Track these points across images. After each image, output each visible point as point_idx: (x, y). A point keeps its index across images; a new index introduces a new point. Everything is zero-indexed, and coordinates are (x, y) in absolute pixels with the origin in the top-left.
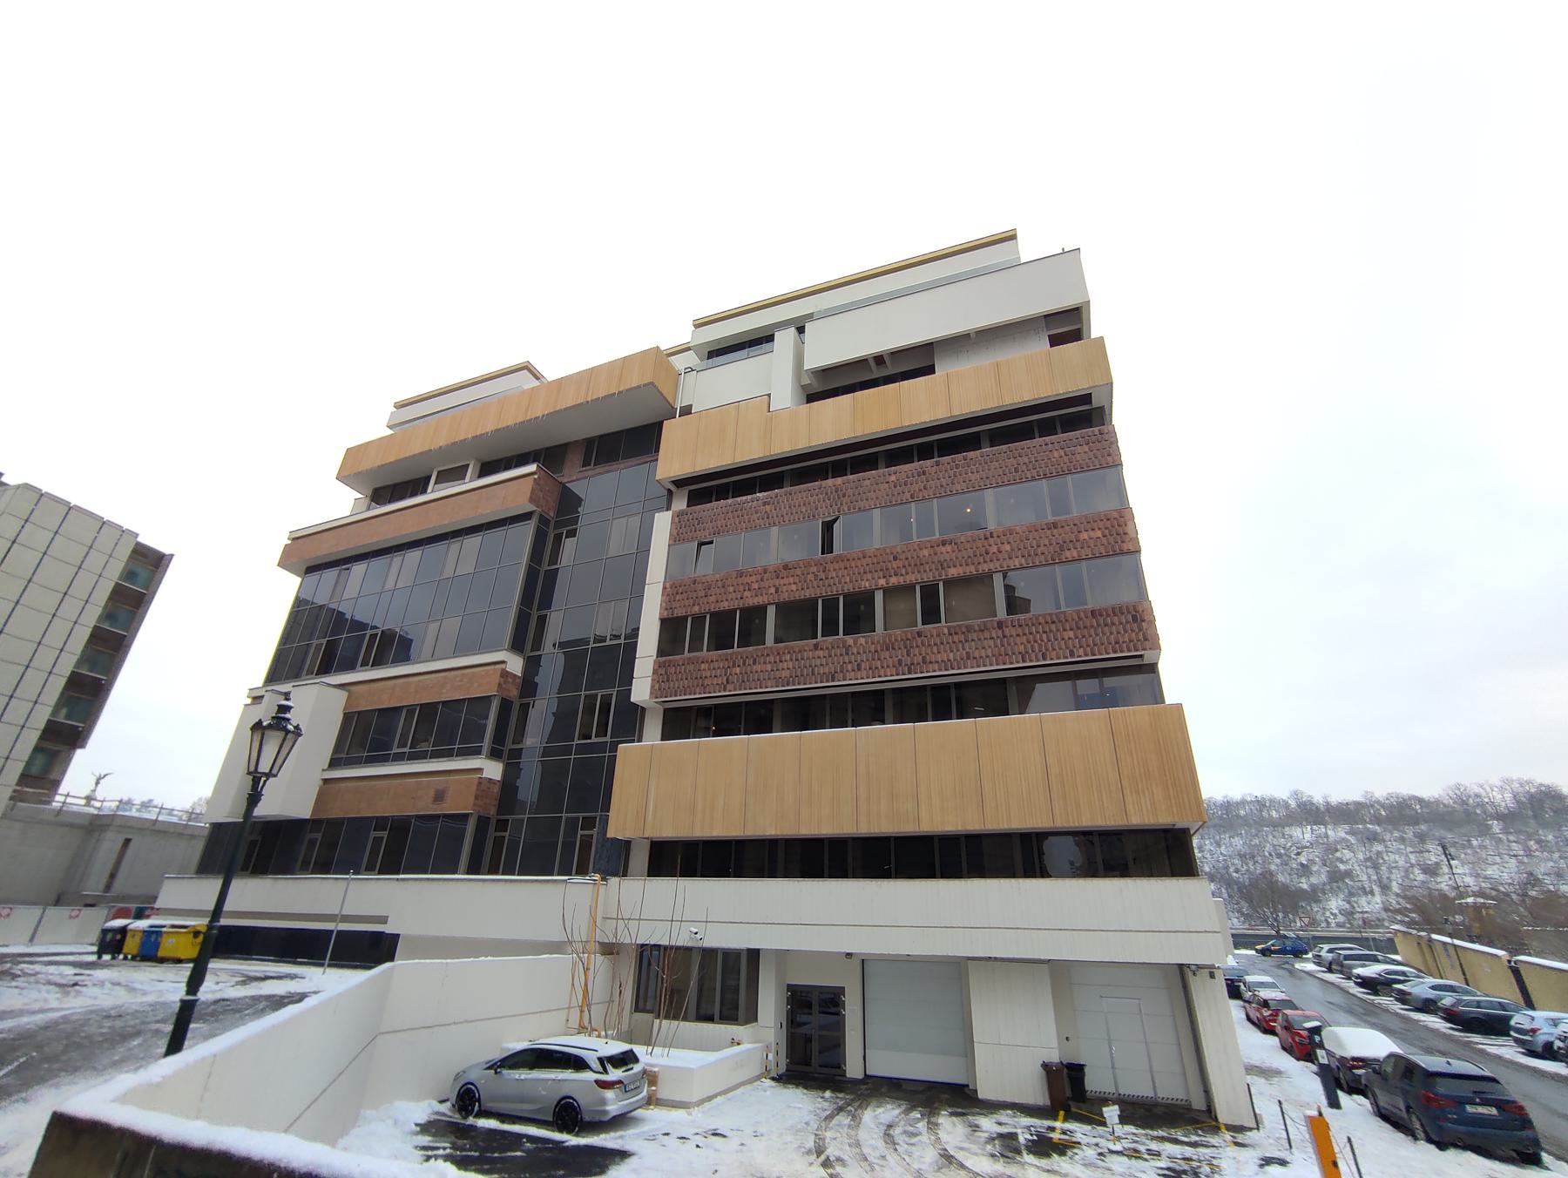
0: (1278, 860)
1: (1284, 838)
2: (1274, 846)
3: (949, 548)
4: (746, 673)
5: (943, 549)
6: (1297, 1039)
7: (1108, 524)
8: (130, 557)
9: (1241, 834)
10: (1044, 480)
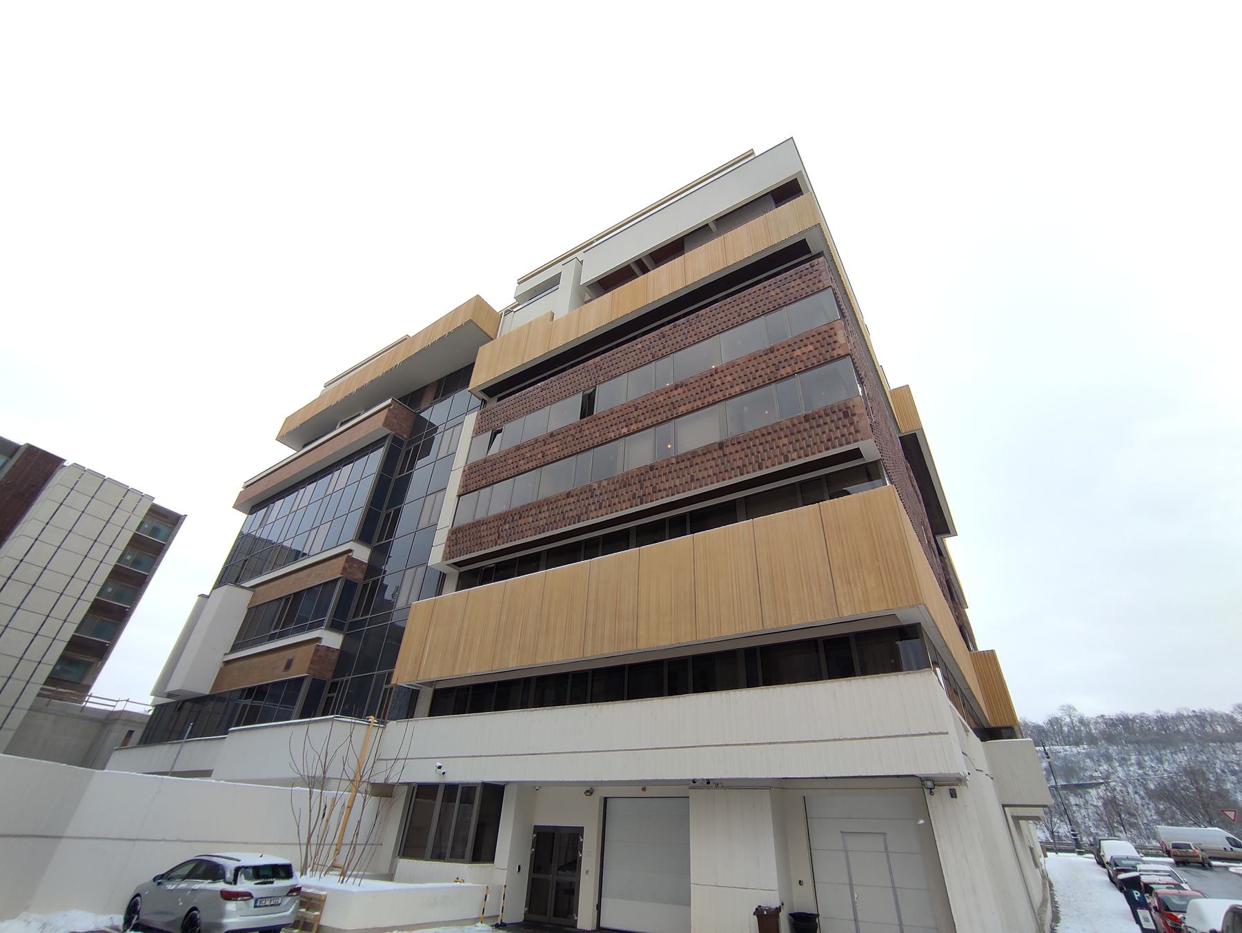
0: (1233, 777)
1: (1236, 754)
2: (1226, 762)
3: (680, 390)
4: (513, 527)
5: (675, 392)
6: (1169, 922)
7: (820, 338)
8: (147, 514)
9: (1184, 749)
10: (763, 317)
